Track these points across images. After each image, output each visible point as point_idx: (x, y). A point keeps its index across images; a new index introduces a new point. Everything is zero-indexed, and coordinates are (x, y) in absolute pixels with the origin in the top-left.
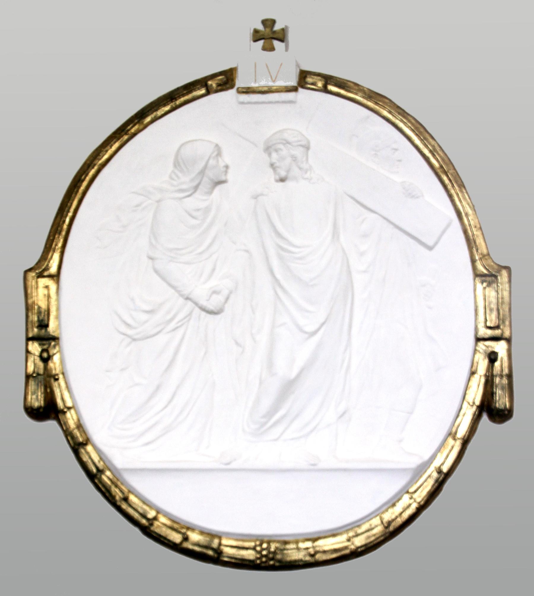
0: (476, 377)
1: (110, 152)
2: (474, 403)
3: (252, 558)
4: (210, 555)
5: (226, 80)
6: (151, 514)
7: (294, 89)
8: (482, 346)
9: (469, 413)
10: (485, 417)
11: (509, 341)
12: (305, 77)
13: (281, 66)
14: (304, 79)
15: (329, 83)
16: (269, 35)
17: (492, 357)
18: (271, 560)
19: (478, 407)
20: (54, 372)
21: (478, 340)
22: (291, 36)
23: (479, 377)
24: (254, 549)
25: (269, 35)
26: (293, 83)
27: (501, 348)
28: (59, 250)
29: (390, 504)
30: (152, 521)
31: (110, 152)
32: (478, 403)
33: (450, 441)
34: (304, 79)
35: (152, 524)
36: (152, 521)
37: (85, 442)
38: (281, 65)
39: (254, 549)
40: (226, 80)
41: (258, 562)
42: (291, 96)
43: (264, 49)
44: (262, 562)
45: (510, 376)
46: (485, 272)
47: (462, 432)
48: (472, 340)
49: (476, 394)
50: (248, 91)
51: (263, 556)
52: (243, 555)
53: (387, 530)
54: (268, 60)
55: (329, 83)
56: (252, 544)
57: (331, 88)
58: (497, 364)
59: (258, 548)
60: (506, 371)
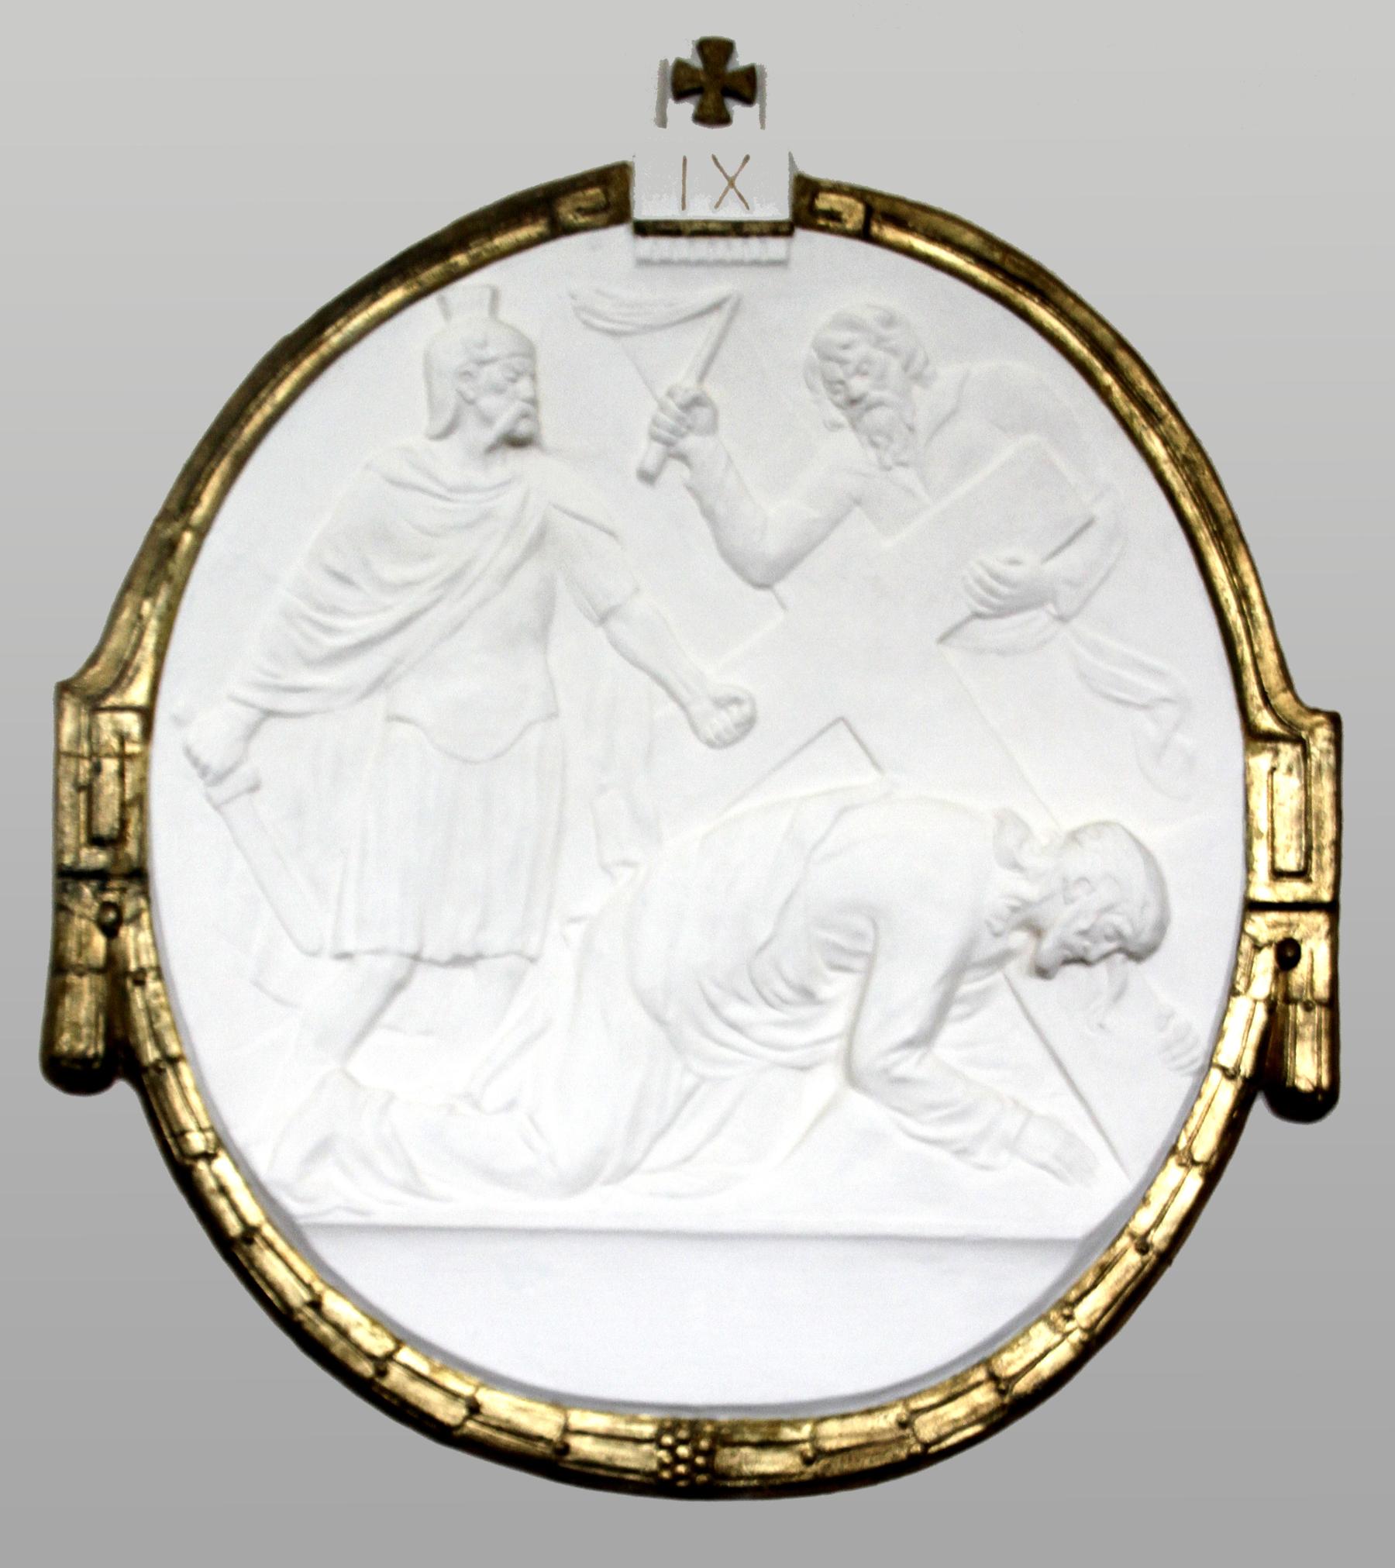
0: (1240, 1006)
1: (281, 393)
2: (1237, 1069)
3: (653, 1465)
4: (552, 1462)
5: (599, 198)
6: (379, 1344)
7: (776, 230)
8: (1262, 926)
9: (1222, 1095)
10: (1260, 1107)
11: (1331, 909)
12: (814, 196)
13: (753, 160)
14: (809, 209)
15: (881, 217)
16: (714, 83)
17: (1288, 954)
18: (698, 1463)
19: (1247, 1081)
20: (133, 966)
21: (1253, 906)
22: (772, 87)
23: (1250, 1004)
24: (655, 1440)
25: (714, 83)
26: (779, 210)
27: (1311, 930)
28: (416, 288)
29: (1019, 1330)
30: (382, 1363)
31: (281, 393)
32: (1246, 1068)
33: (1173, 1171)
34: (806, 189)
35: (382, 1373)
36: (382, 1363)
37: (211, 1151)
38: (715, 159)
39: (655, 1440)
40: (599, 198)
41: (666, 1474)
42: (775, 247)
43: (701, 118)
44: (677, 1477)
45: (1332, 1004)
46: (1276, 728)
47: (1205, 1147)
48: (1235, 906)
49: (1240, 1048)
50: (643, 229)
51: (678, 1460)
52: (427, 1402)
53: (1007, 1400)
54: (676, 165)
55: (881, 217)
56: (648, 1430)
57: (891, 234)
58: (1302, 968)
59: (668, 1440)
60: (1322, 990)
